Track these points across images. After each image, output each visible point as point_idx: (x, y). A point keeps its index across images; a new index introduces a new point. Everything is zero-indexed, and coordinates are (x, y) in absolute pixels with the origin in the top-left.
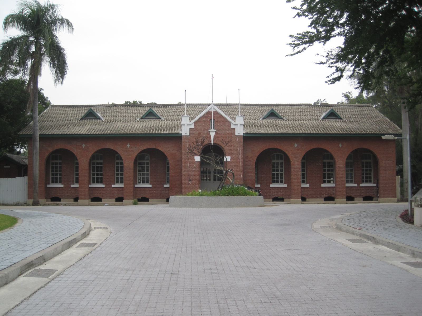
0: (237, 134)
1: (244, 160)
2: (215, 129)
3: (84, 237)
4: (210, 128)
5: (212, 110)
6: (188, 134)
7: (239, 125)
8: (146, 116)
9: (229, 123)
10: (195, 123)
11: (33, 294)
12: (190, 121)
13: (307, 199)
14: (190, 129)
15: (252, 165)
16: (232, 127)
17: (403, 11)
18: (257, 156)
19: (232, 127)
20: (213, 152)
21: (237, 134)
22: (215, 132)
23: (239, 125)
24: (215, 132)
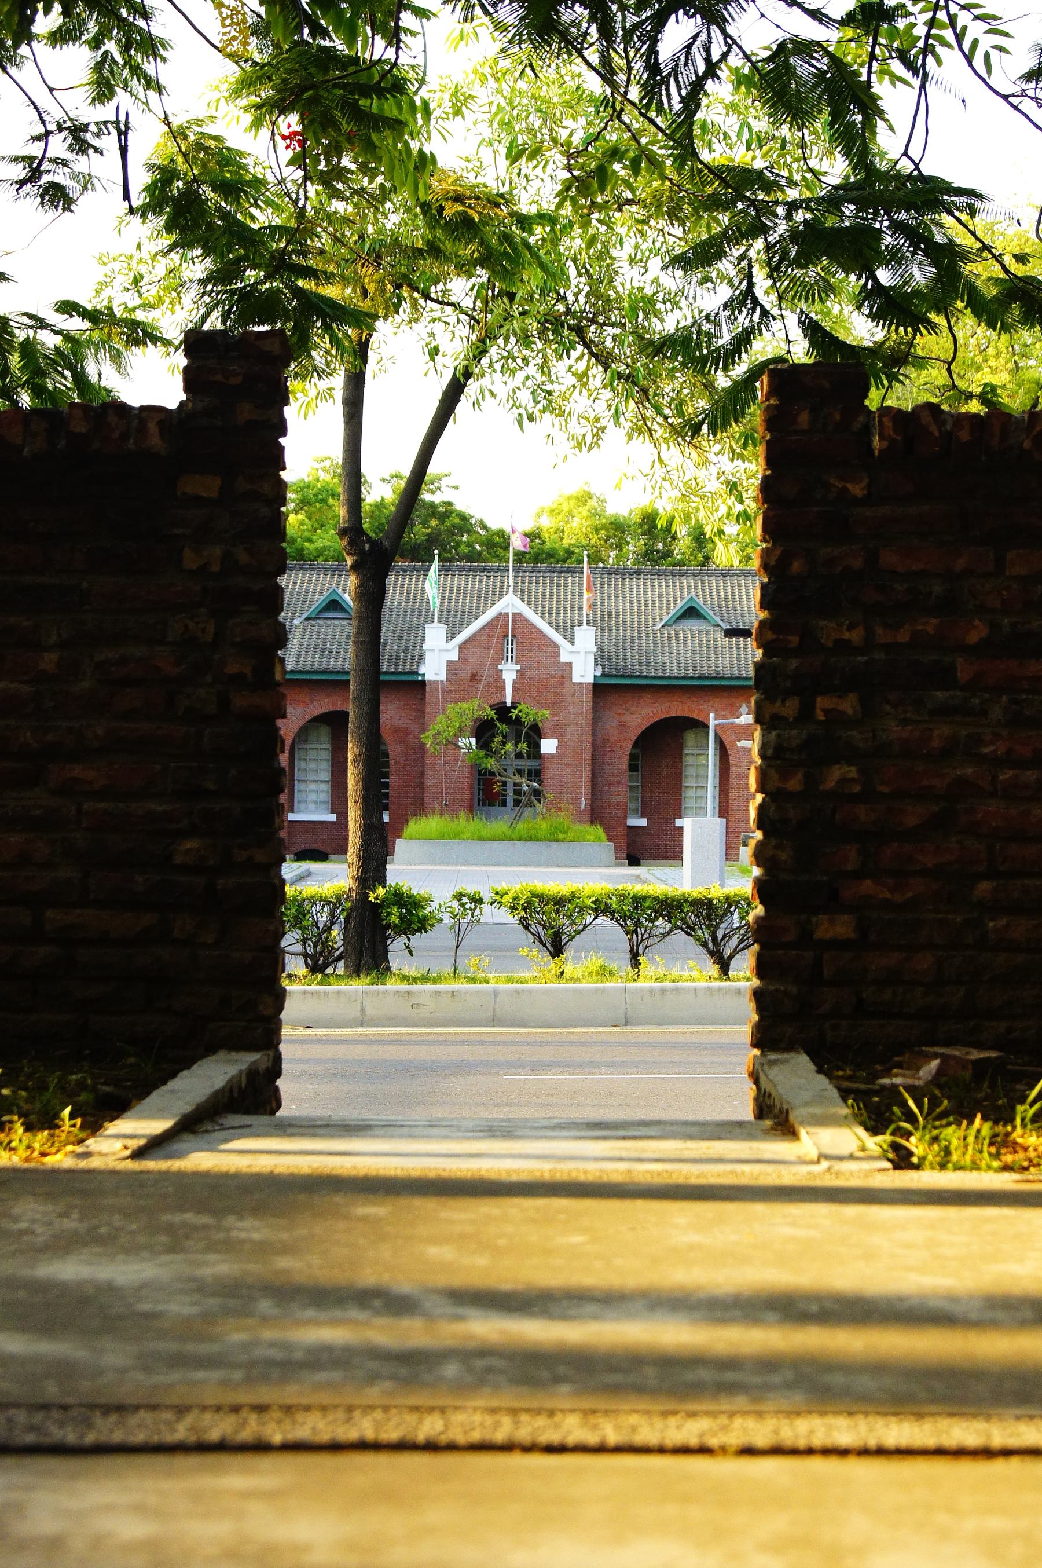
0: (576, 679)
1: (594, 748)
2: (517, 663)
3: (142, 1176)
4: (500, 659)
5: (510, 611)
6: (443, 677)
7: (436, 651)
8: (321, 611)
9: (556, 647)
10: (462, 646)
11: (794, 1452)
12: (451, 637)
13: (331, 857)
14: (571, 663)
15: (619, 762)
16: (564, 658)
17: (170, 393)
18: (635, 738)
19: (564, 658)
20: (499, 726)
21: (576, 679)
22: (517, 671)
23: (436, 651)
24: (517, 671)
